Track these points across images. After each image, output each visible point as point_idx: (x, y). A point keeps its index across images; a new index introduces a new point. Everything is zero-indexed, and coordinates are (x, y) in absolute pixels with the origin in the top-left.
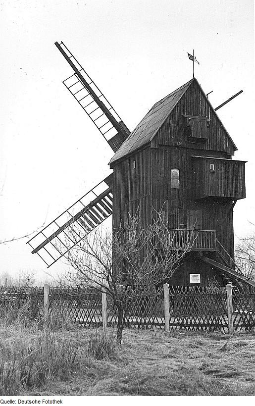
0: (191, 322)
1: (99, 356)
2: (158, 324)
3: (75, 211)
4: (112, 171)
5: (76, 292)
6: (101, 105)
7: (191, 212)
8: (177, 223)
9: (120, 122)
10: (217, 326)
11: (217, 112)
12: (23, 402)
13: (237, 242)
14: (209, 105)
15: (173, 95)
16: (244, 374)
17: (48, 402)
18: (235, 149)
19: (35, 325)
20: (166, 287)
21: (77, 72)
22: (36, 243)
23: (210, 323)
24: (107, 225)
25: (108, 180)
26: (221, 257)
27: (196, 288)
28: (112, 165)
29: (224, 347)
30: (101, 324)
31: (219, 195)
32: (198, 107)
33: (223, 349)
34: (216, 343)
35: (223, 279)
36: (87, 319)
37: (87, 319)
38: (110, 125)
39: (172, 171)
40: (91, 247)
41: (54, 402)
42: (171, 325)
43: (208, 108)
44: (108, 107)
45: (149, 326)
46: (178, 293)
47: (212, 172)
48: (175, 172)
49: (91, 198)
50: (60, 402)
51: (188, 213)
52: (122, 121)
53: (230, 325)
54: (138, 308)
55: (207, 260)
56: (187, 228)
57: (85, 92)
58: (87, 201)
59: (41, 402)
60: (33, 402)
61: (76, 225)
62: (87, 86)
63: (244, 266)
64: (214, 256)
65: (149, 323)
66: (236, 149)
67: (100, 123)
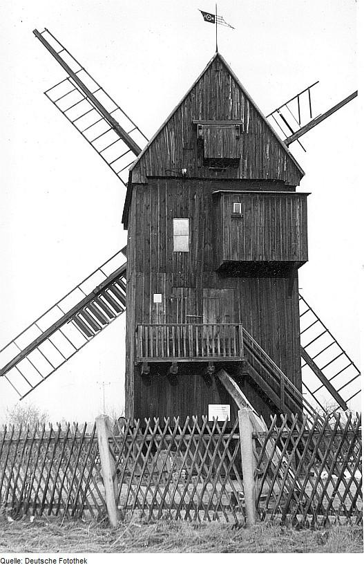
0: (182, 499)
3: (68, 305)
7: (212, 292)
8: (184, 316)
12: (32, 561)
17: (67, 561)
21: (72, 75)
32: (226, 105)
41: (75, 561)
47: (237, 217)
49: (99, 279)
50: (83, 561)
51: (205, 295)
57: (86, 105)
58: (89, 288)
59: (58, 561)
60: (47, 562)
61: (70, 328)
62: (89, 96)
64: (269, 369)
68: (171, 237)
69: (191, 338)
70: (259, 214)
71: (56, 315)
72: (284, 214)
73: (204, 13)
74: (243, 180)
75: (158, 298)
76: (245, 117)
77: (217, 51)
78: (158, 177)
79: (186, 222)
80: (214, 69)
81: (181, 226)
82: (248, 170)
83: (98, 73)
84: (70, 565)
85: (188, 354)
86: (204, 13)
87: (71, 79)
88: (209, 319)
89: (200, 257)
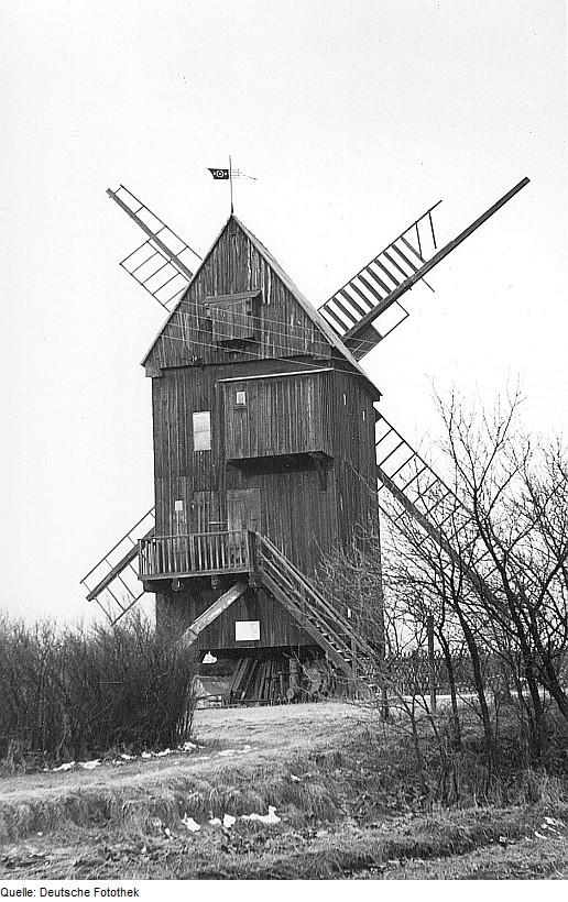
12: (50, 893)
17: (107, 893)
18: (376, 395)
22: (93, 582)
32: (245, 273)
41: (120, 892)
43: (266, 268)
47: (241, 409)
50: (133, 893)
59: (92, 893)
60: (74, 893)
66: (376, 395)
68: (191, 435)
69: (192, 550)
70: (266, 401)
72: (293, 399)
74: (265, 359)
75: (179, 505)
76: (266, 285)
78: (175, 368)
79: (207, 415)
80: (229, 233)
81: (202, 420)
85: (190, 569)
87: (152, 242)
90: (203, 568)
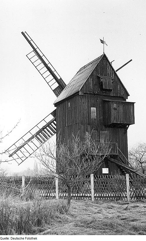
1: (61, 213)
2: (87, 197)
4: (56, 108)
5: (45, 179)
6: (49, 69)
9: (60, 79)
10: (120, 198)
11: (117, 73)
12: (13, 239)
13: (129, 149)
14: (113, 69)
15: (92, 63)
16: (140, 220)
17: (29, 238)
19: (18, 197)
20: (92, 176)
21: (35, 50)
23: (103, 196)
24: (53, 139)
25: (54, 113)
26: (120, 158)
27: (109, 176)
28: (56, 105)
29: (126, 208)
30: (54, 197)
31: (119, 123)
32: (107, 71)
33: (126, 209)
34: (121, 206)
35: (123, 171)
36: (47, 195)
37: (47, 195)
38: (54, 81)
39: (92, 108)
40: (53, 154)
41: (32, 238)
42: (95, 197)
44: (53, 70)
45: (82, 198)
46: (98, 179)
47: (115, 109)
48: (93, 109)
49: (44, 124)
52: (61, 78)
53: (128, 196)
54: (76, 188)
55: (112, 160)
56: (101, 141)
57: (39, 61)
58: (41, 126)
59: (25, 239)
60: (20, 239)
61: (35, 140)
63: (133, 163)
64: (117, 160)
65: (82, 196)
66: (128, 95)
67: (48, 79)
71: (29, 136)
73: (101, 40)
74: (112, 96)
76: (112, 75)
77: (104, 53)
82: (113, 93)
83: (43, 50)
84: (30, 240)
86: (101, 40)
88: (102, 141)
89: (99, 120)
90: (112, 153)
